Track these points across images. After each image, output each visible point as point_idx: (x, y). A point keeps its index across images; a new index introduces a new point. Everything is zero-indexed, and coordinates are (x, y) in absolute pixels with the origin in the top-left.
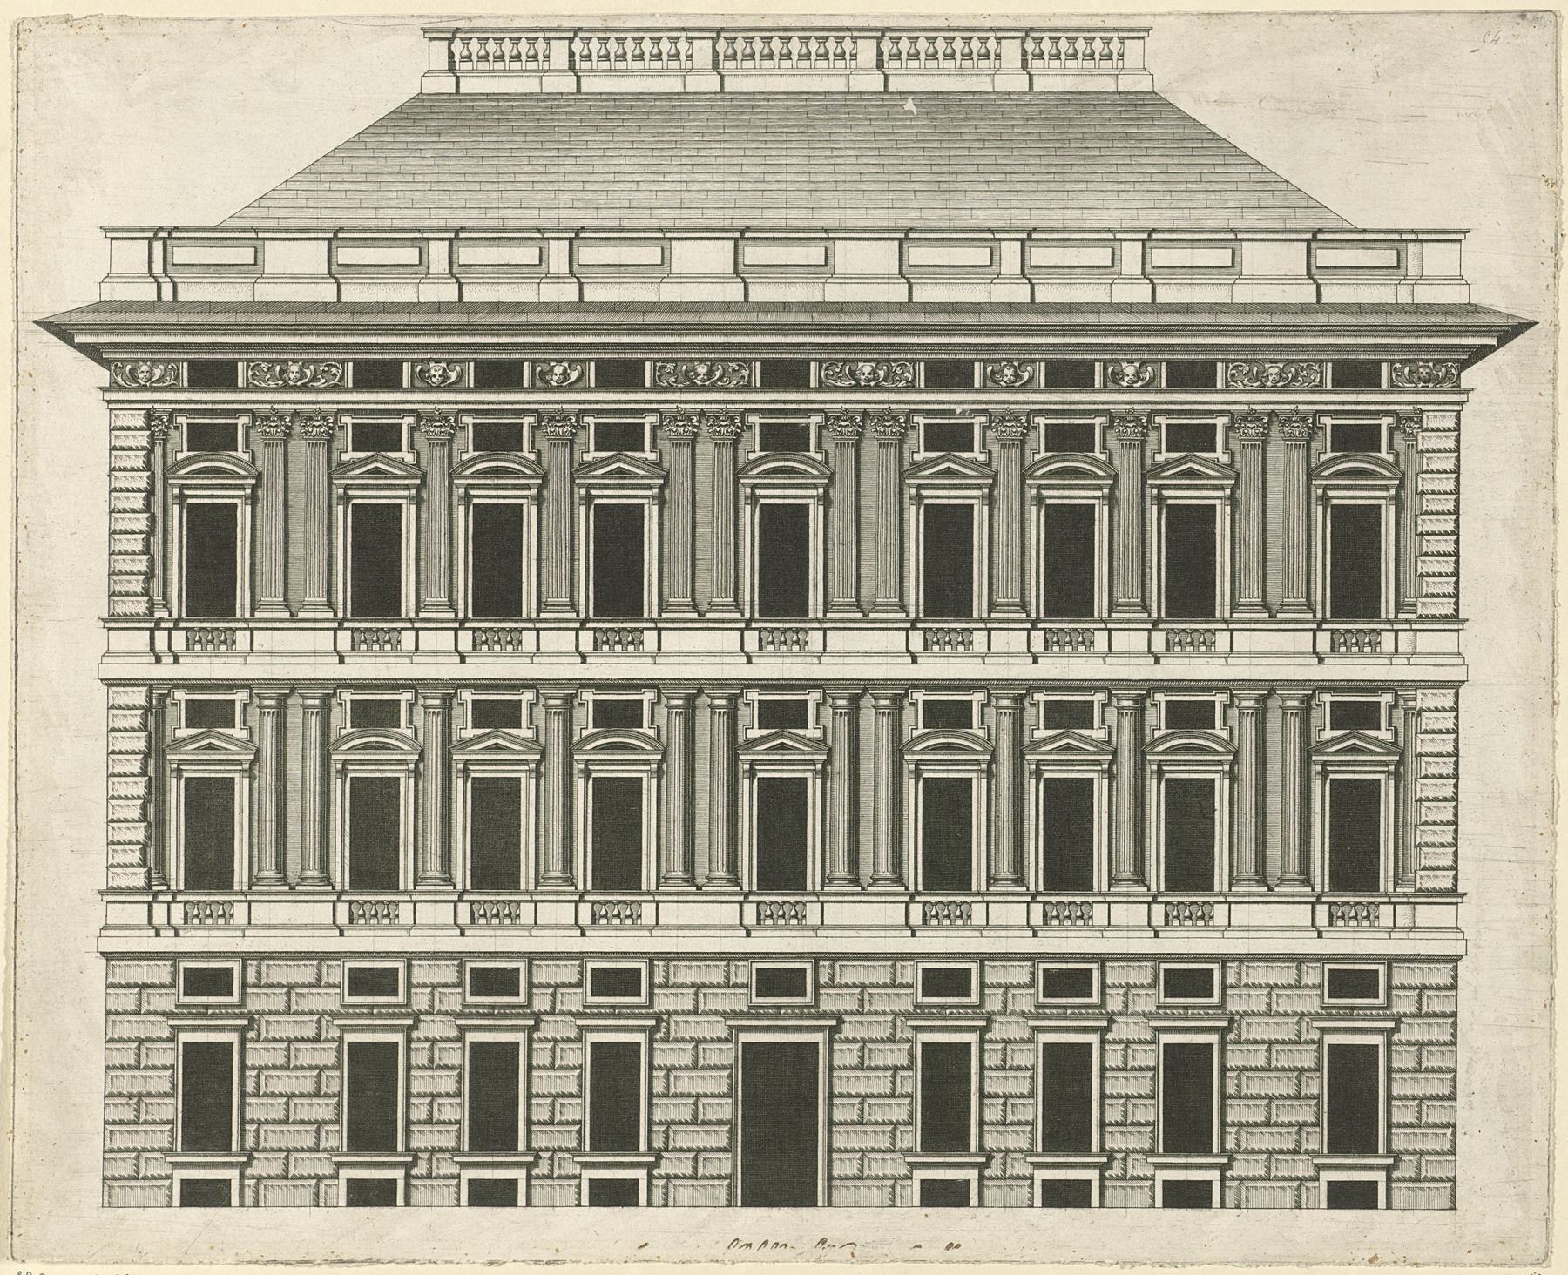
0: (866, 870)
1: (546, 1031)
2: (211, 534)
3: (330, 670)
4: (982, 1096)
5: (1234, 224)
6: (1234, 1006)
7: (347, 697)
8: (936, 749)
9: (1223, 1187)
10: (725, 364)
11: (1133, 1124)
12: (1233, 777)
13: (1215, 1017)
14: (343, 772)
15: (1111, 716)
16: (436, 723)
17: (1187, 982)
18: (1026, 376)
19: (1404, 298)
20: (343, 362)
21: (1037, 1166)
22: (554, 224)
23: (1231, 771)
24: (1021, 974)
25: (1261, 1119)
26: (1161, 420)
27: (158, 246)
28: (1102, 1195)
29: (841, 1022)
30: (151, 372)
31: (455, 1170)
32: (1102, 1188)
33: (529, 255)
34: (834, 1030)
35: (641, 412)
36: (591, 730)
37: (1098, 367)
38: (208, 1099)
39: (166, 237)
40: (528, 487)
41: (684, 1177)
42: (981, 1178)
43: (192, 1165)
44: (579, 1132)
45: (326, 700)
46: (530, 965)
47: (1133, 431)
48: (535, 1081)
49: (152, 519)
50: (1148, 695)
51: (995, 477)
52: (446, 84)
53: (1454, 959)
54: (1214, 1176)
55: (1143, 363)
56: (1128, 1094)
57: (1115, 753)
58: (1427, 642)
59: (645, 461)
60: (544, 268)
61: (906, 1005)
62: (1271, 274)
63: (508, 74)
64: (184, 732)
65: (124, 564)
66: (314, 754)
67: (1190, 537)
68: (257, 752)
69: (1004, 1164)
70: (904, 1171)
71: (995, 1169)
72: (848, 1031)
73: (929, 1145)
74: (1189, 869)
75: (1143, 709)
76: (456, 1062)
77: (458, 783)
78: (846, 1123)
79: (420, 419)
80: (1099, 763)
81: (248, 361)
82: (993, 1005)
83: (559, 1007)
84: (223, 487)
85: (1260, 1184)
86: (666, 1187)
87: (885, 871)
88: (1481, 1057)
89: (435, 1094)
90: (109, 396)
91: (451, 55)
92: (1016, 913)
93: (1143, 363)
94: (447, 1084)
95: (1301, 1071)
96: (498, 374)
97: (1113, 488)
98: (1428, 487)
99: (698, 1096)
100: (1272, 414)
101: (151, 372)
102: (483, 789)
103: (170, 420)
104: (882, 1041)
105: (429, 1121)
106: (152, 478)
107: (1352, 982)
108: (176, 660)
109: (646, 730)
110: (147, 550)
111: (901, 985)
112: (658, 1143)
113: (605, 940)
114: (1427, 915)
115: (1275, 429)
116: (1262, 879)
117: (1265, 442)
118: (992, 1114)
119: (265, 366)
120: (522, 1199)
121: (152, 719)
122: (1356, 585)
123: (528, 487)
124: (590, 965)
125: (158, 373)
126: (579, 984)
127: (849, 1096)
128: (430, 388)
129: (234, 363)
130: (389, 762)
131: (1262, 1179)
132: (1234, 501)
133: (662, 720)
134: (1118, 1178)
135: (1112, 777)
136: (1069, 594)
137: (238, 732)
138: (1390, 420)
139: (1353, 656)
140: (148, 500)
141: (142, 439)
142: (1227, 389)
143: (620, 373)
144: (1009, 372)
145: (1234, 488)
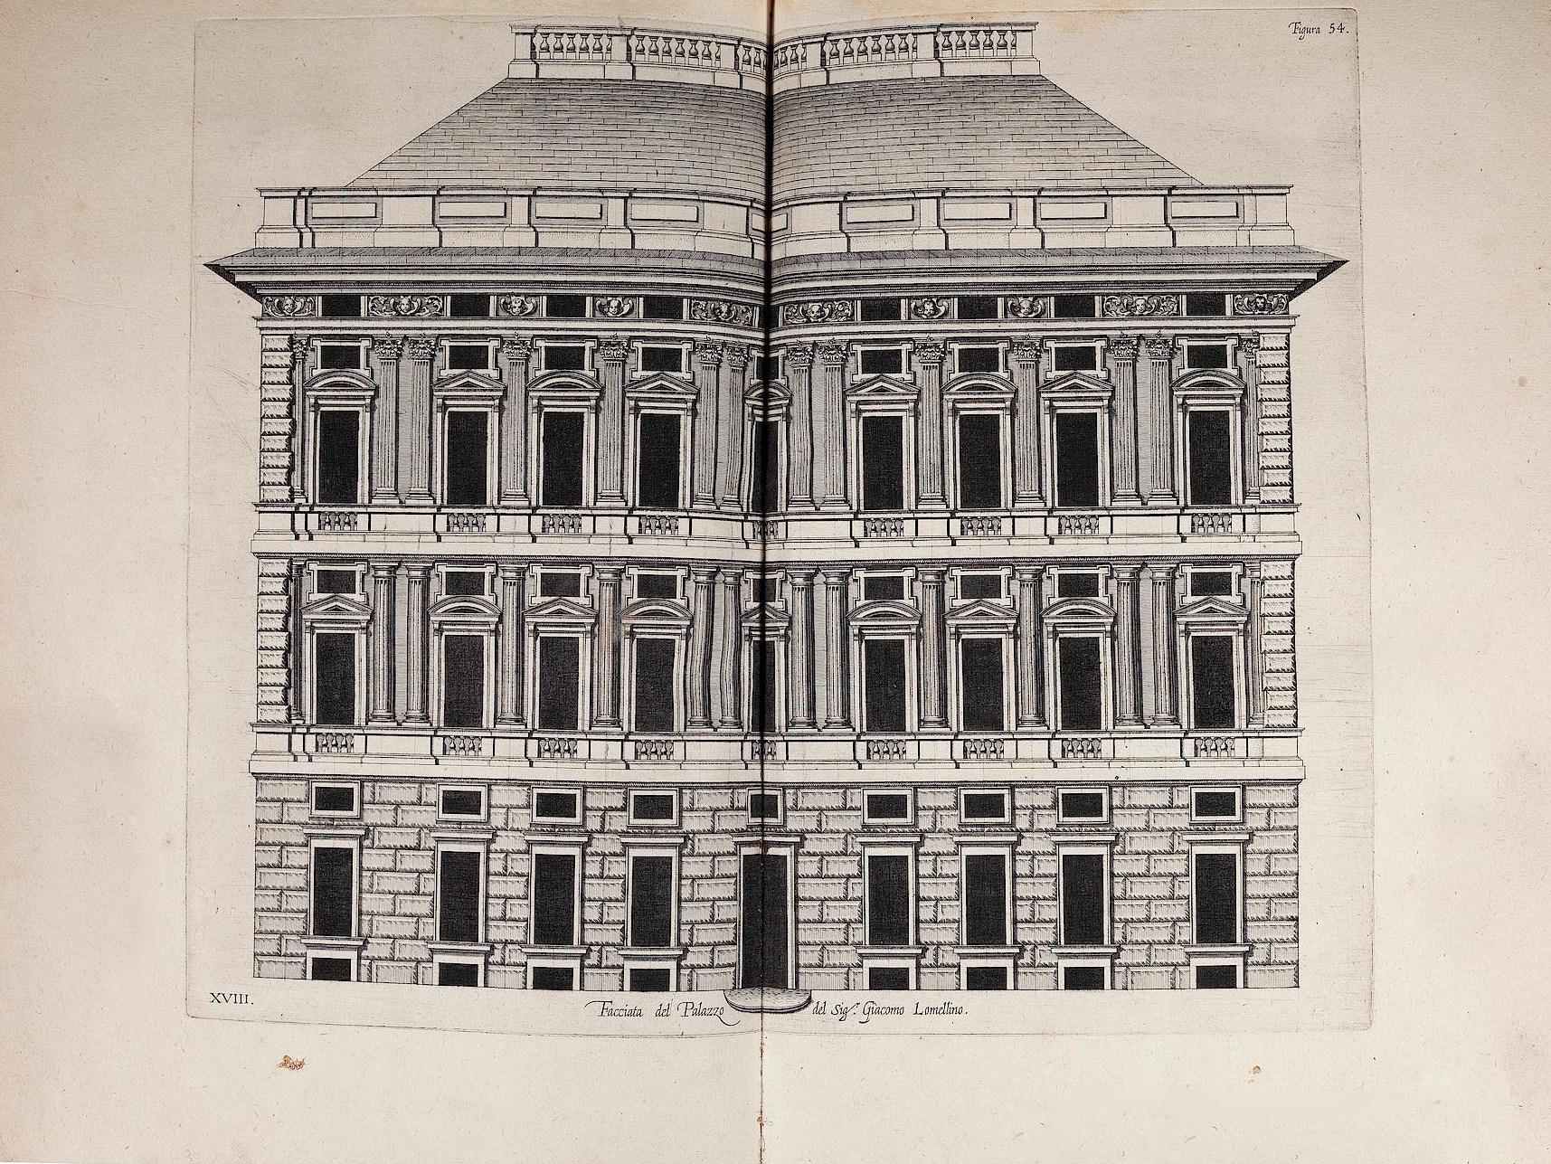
0: (821, 715)
1: (929, 846)
2: (339, 437)
3: (430, 548)
4: (918, 899)
5: (1106, 183)
6: (1119, 823)
7: (443, 569)
8: (876, 616)
9: (1113, 971)
10: (1157, 297)
11: (1040, 921)
12: (1114, 636)
13: (1103, 833)
14: (440, 631)
15: (1015, 585)
16: (512, 592)
17: (1081, 804)
18: (943, 310)
19: (1243, 242)
20: (443, 296)
21: (962, 956)
22: (612, 185)
23: (1112, 631)
24: (946, 799)
25: (1142, 916)
26: (1051, 344)
27: (301, 202)
28: (1016, 980)
29: (803, 839)
30: (294, 305)
31: (523, 959)
32: (1016, 973)
33: (591, 209)
34: (800, 845)
35: (680, 340)
36: (636, 599)
37: (1000, 301)
38: (333, 898)
39: (305, 195)
40: (588, 399)
41: (705, 967)
42: (918, 966)
43: (976, 956)
44: (622, 930)
45: (427, 570)
46: (489, 790)
47: (1029, 355)
48: (587, 887)
49: (294, 424)
50: (1044, 570)
51: (919, 393)
52: (528, 71)
53: (1295, 783)
54: (1105, 963)
55: (1036, 297)
56: (1036, 899)
57: (1018, 618)
58: (1269, 523)
59: (682, 380)
60: (603, 222)
61: (855, 825)
62: (1135, 225)
63: (578, 63)
64: (316, 596)
65: (271, 460)
66: (417, 615)
67: (1077, 439)
68: (373, 614)
69: (936, 955)
70: (1183, 959)
71: (929, 959)
72: (810, 846)
73: (875, 940)
74: (1081, 710)
75: (1041, 581)
76: (525, 871)
77: (529, 641)
78: (809, 922)
79: (503, 342)
80: (1006, 626)
81: (369, 296)
82: (925, 824)
83: (607, 827)
84: (348, 398)
85: (1142, 969)
86: (690, 975)
87: (837, 717)
88: (1319, 866)
89: (508, 899)
90: (261, 324)
91: (533, 47)
92: (1039, 749)
93: (1036, 297)
94: (948, 890)
95: (1174, 876)
96: (566, 306)
97: (1014, 401)
98: (1266, 396)
99: (714, 900)
100: (1140, 337)
101: (294, 305)
102: (970, 649)
103: (308, 343)
104: (837, 854)
105: (503, 919)
106: (293, 390)
107: (1214, 803)
108: (311, 538)
109: (907, 601)
110: (289, 449)
111: (851, 809)
112: (685, 939)
113: (976, 771)
114: (1274, 747)
115: (1143, 349)
116: (1140, 719)
117: (1135, 361)
118: (926, 914)
119: (382, 299)
120: (1240, 982)
121: (292, 586)
122: (1210, 484)
123: (588, 399)
124: (633, 793)
125: (299, 305)
126: (624, 809)
127: (811, 899)
128: (512, 317)
129: (358, 296)
130: (474, 623)
131: (1144, 965)
132: (1111, 411)
133: (690, 593)
134: (1029, 966)
135: (1016, 637)
136: (981, 487)
137: (358, 597)
138: (1103, 343)
139: (1210, 535)
140: (290, 407)
141: (286, 359)
142: (1104, 317)
143: (663, 307)
144: (929, 307)
145: (695, 402)
